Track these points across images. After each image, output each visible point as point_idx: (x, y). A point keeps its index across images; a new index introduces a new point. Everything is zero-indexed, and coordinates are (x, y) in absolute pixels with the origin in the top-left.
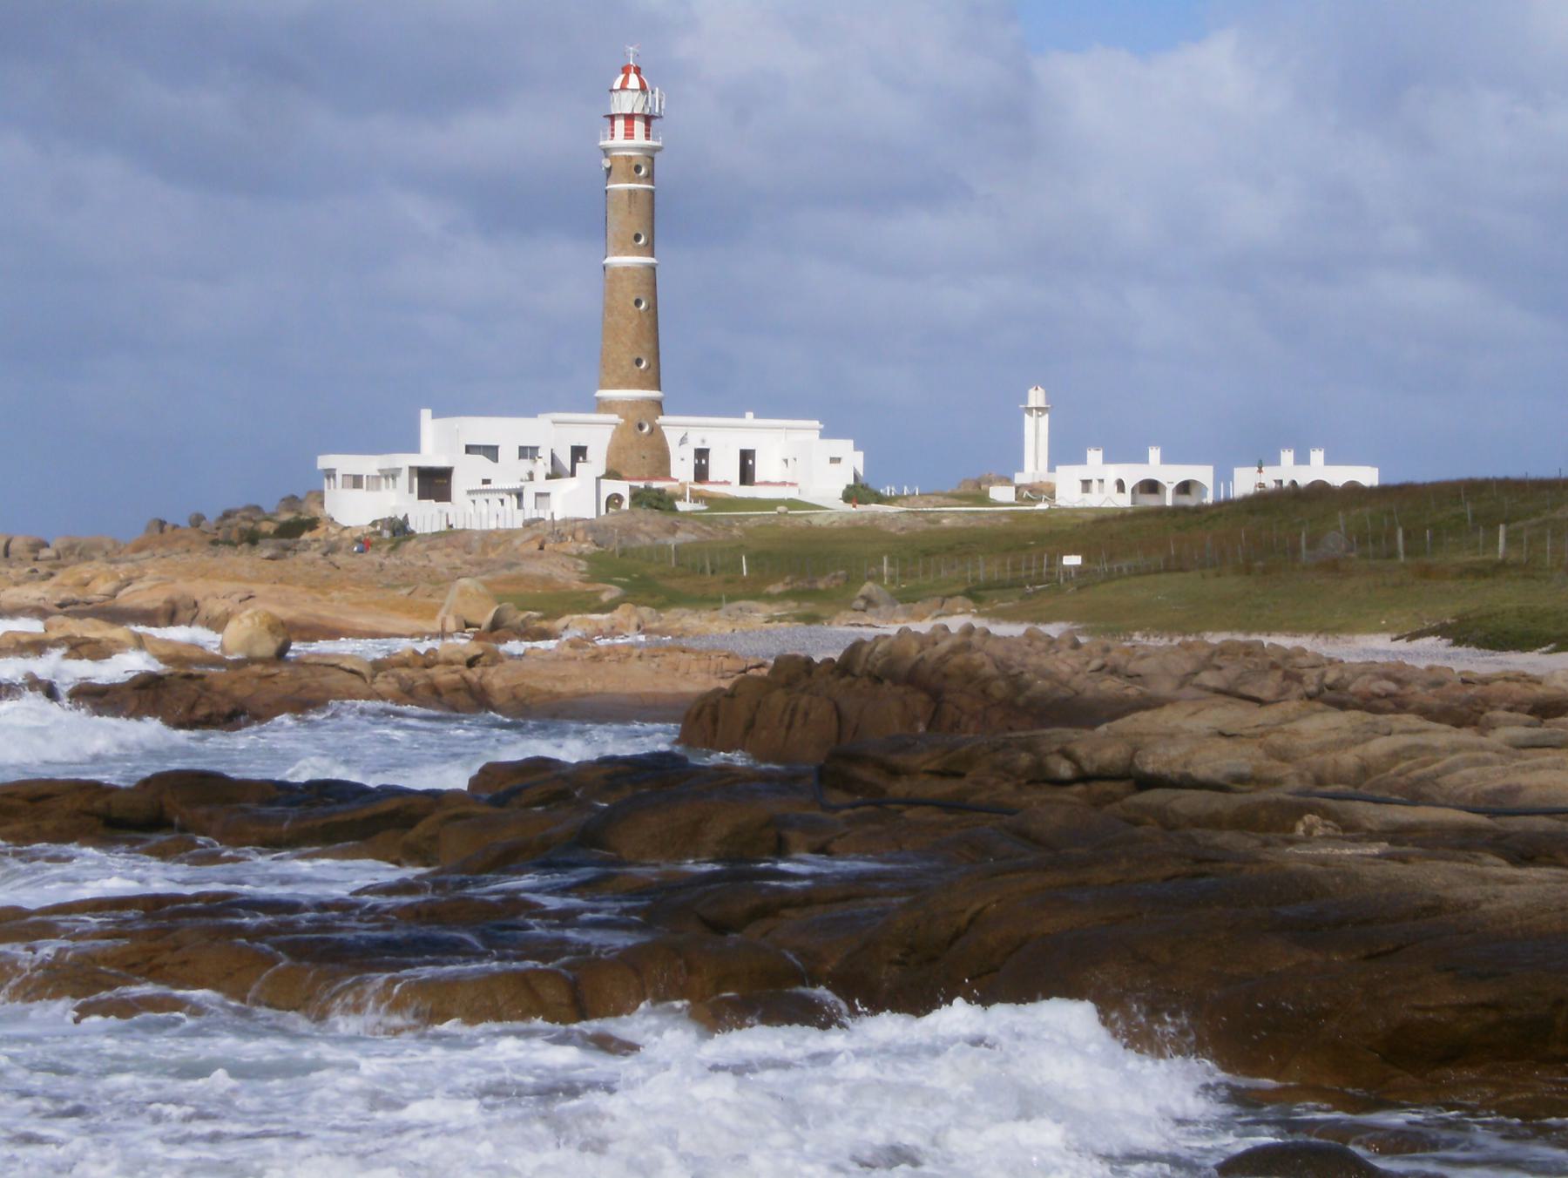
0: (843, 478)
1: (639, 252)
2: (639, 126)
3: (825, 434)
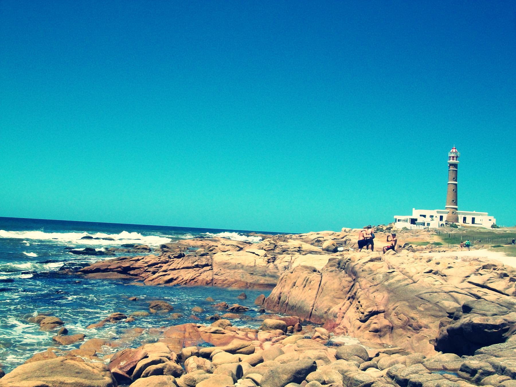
0: (491, 223)
1: (454, 181)
2: (455, 158)
3: (489, 215)
